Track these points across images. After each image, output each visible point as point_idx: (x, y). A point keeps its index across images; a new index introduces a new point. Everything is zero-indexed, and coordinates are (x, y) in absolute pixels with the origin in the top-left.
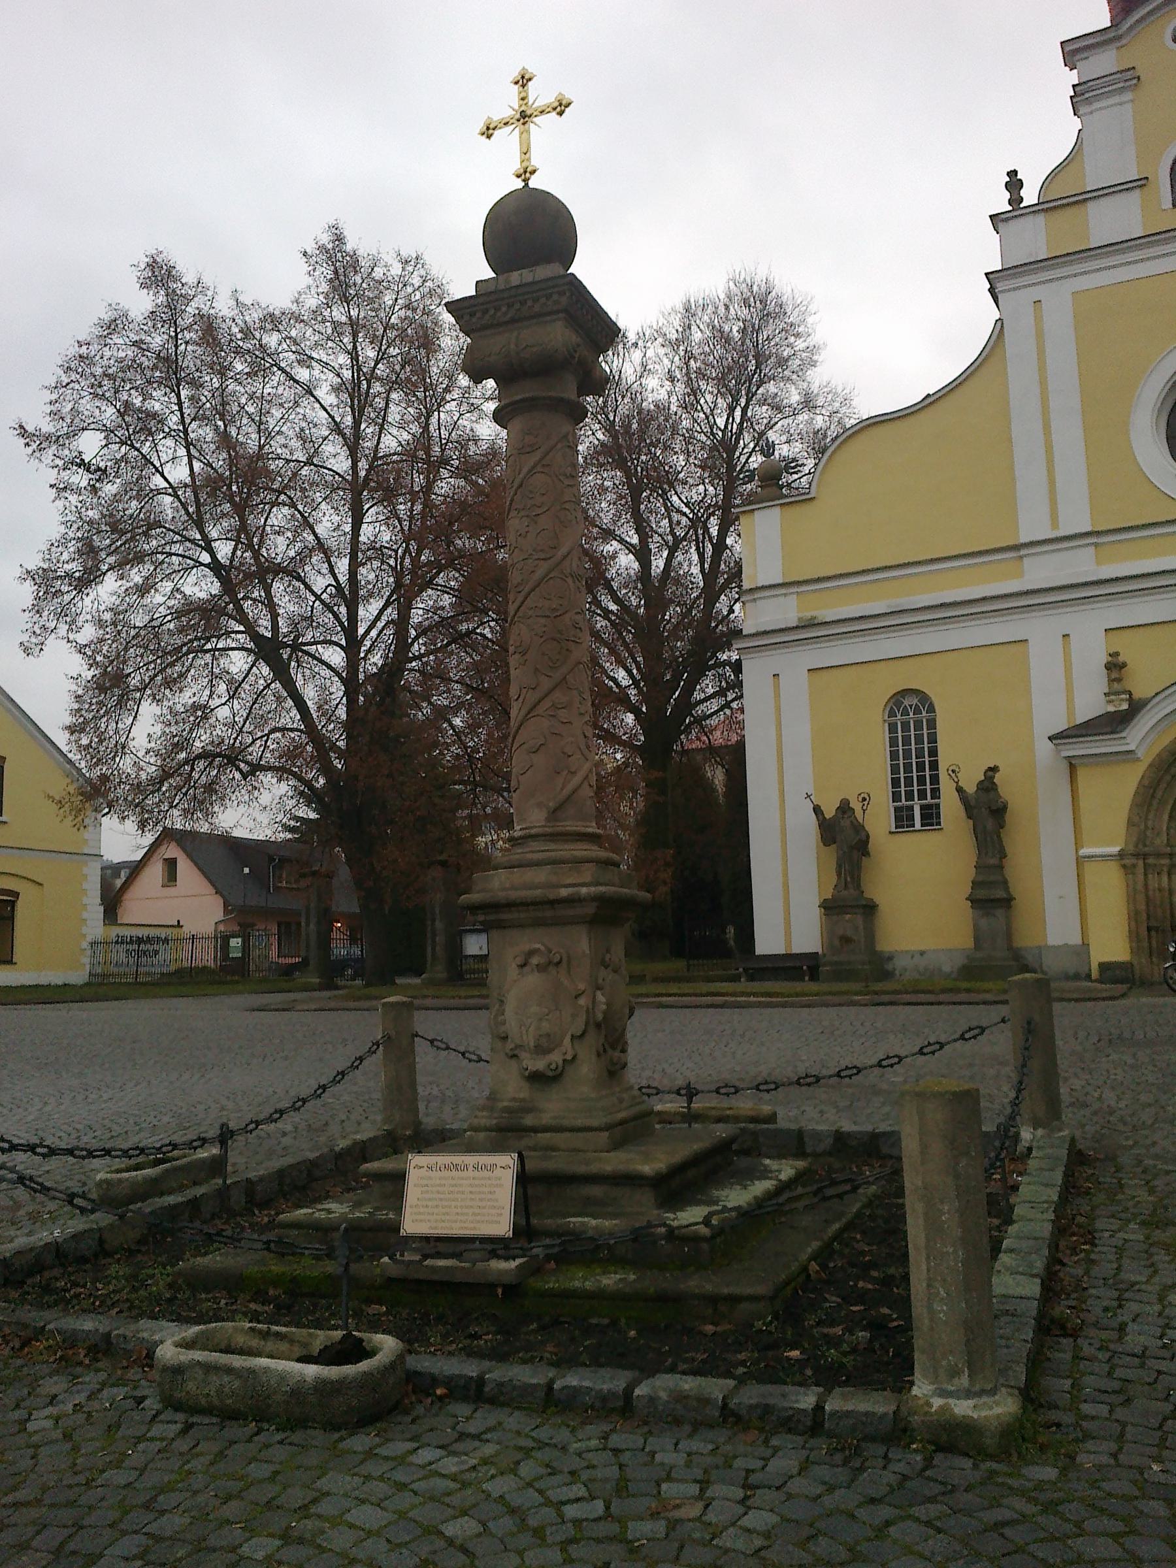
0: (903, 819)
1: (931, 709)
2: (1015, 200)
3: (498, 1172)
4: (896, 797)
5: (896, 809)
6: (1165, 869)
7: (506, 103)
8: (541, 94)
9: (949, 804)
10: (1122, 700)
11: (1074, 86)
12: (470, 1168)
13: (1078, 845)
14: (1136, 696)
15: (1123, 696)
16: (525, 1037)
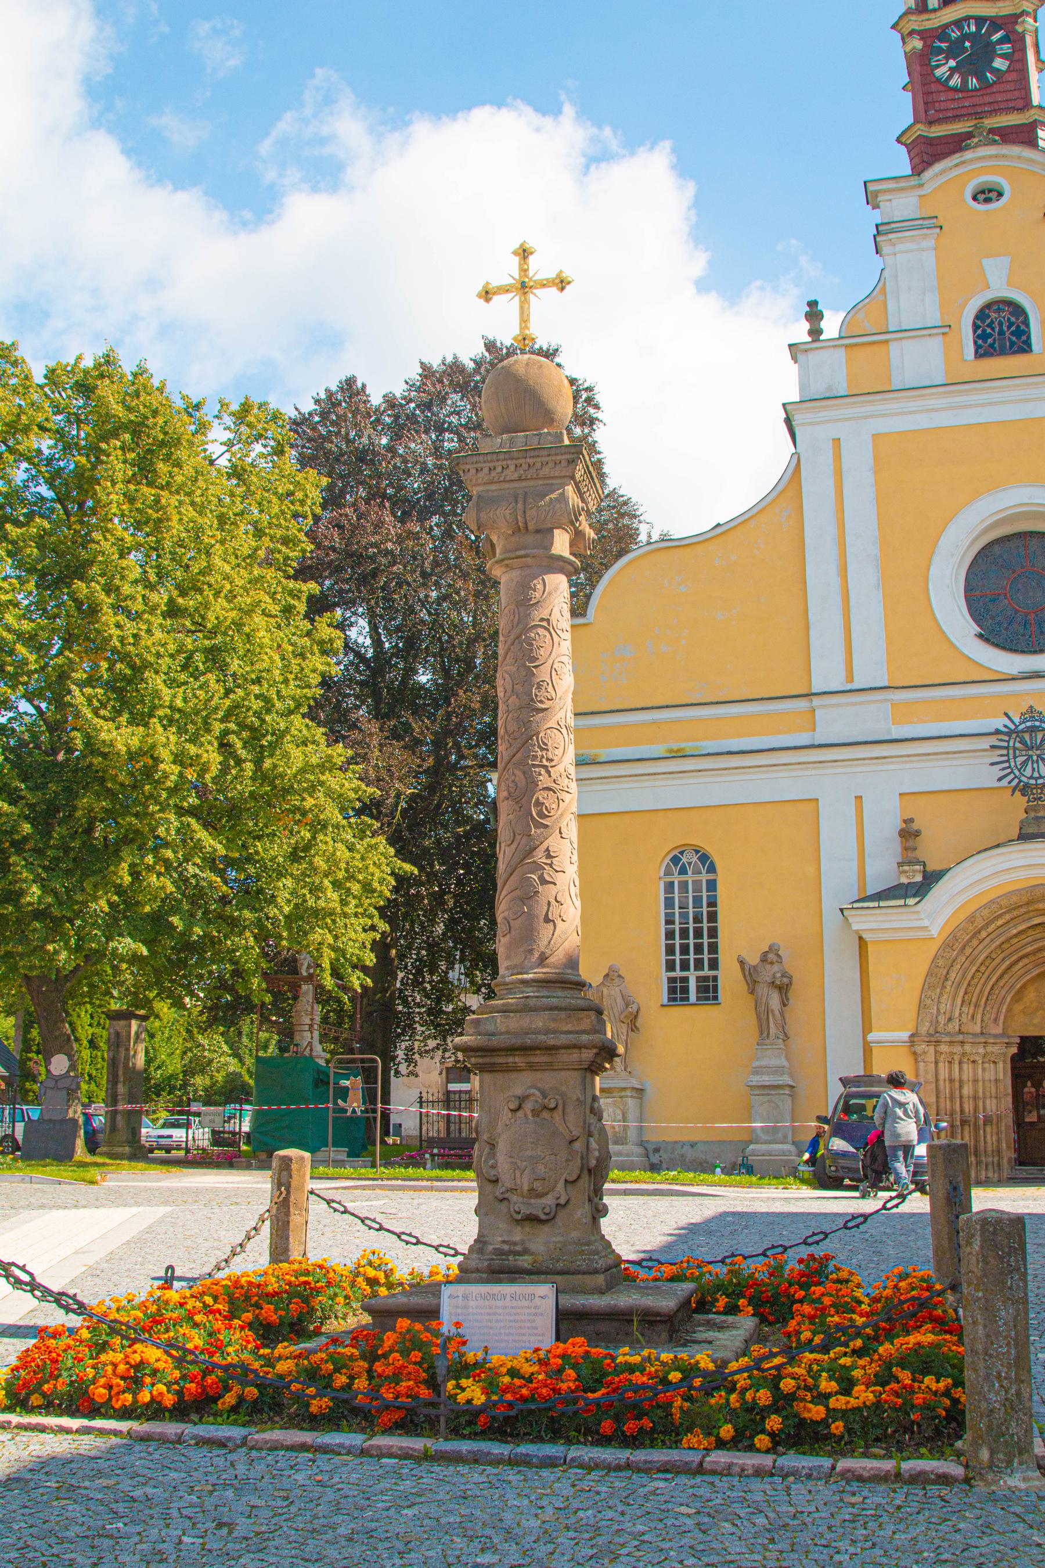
0: (677, 992)
1: (712, 869)
2: (815, 333)
3: (537, 1301)
4: (670, 966)
5: (672, 980)
6: (957, 1058)
7: (507, 271)
8: (540, 267)
9: (729, 976)
10: (914, 871)
11: (877, 226)
12: (508, 1298)
13: (867, 1027)
14: (929, 868)
15: (917, 867)
16: (518, 1181)
